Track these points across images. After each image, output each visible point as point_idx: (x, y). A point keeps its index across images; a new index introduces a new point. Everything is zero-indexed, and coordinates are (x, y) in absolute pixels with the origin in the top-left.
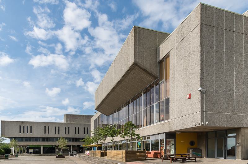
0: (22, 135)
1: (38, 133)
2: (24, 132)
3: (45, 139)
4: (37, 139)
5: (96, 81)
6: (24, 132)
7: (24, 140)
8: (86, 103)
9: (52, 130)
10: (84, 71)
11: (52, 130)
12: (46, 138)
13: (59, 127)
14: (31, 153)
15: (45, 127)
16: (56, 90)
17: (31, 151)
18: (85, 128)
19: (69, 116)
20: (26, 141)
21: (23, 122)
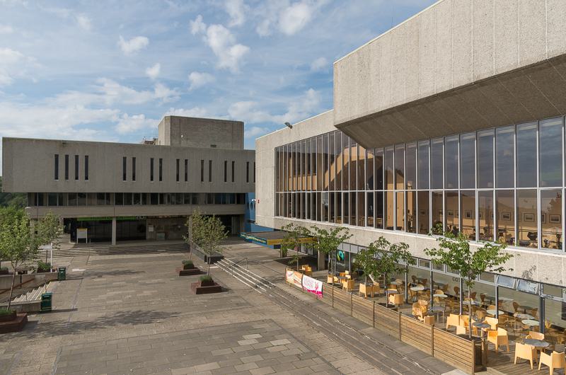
0: (63, 186)
1: (105, 180)
2: (67, 178)
3: (121, 199)
4: (103, 197)
5: (231, 24)
6: (67, 178)
7: (46, 200)
8: (195, 77)
9: (143, 171)
10: (493, 327)
11: (143, 171)
12: (185, 194)
13: (161, 160)
14: (82, 241)
15: (125, 159)
16: (140, 41)
17: (82, 233)
18: (226, 162)
19: (178, 125)
20: (218, 202)
21: (64, 144)
